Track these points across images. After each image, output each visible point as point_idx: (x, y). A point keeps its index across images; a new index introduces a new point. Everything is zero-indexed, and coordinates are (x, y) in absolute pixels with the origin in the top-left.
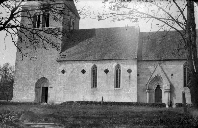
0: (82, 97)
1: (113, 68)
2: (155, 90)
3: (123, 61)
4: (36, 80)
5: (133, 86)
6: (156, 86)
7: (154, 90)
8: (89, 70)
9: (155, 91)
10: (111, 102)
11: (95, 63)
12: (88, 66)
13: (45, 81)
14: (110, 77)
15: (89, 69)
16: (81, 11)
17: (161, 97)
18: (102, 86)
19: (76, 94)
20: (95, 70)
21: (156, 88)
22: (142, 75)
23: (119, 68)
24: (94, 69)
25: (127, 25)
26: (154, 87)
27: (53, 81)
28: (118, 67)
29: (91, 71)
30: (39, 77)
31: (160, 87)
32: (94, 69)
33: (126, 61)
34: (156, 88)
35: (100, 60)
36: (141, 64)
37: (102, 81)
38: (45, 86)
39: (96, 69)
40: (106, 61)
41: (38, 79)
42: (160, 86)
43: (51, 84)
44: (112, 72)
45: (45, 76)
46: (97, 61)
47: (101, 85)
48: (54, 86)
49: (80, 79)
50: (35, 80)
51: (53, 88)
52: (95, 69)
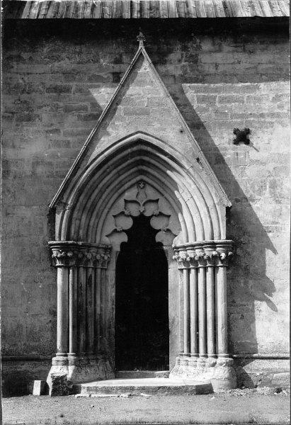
2: (117, 248)
6: (127, 223)
7: (108, 249)
21: (125, 238)
34: (125, 238)
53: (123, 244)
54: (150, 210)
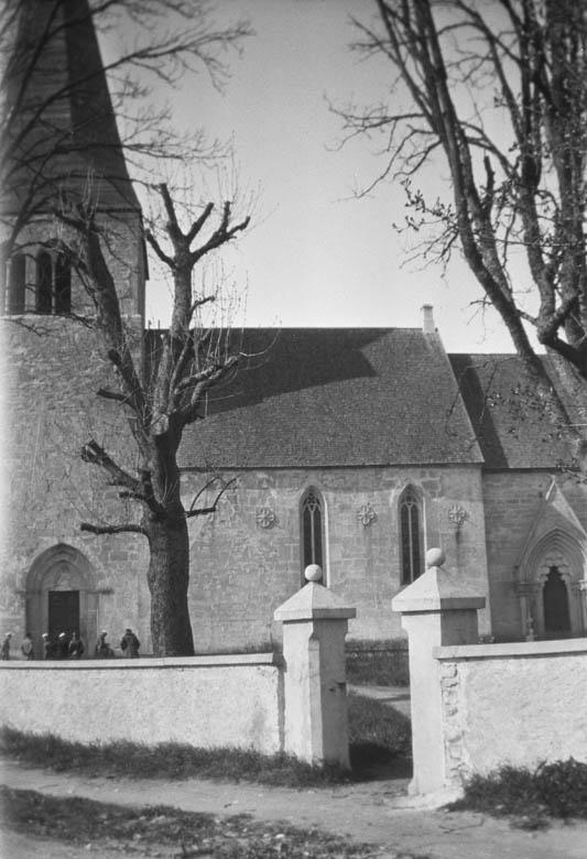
0: (263, 629)
1: (391, 500)
2: (543, 585)
3: (427, 471)
4: (24, 559)
5: (474, 573)
6: (547, 571)
7: (539, 584)
8: (291, 511)
9: (545, 591)
10: (144, 301)
11: (313, 479)
12: (285, 500)
13: (62, 564)
14: (382, 540)
15: (288, 507)
16: (229, 170)
17: (566, 613)
18: (347, 576)
19: (233, 618)
20: (312, 512)
21: (546, 579)
22: (498, 530)
23: (412, 503)
24: (307, 509)
25: (513, 153)
26: (539, 574)
27: (110, 562)
28: (410, 496)
29: (297, 515)
30: (38, 544)
31: (561, 575)
32: (308, 505)
33: (440, 472)
34: (546, 579)
35: (337, 467)
36: (492, 486)
37: (348, 556)
38: (64, 586)
39: (317, 509)
40: (360, 475)
41: (37, 553)
42: (561, 570)
43: (101, 576)
44: (389, 517)
45: (69, 541)
46: (321, 473)
47: (343, 575)
48: (119, 586)
49: (249, 552)
50: (19, 559)
51: (114, 597)
52: (312, 507)
53: (546, 583)
54: (558, 563)
